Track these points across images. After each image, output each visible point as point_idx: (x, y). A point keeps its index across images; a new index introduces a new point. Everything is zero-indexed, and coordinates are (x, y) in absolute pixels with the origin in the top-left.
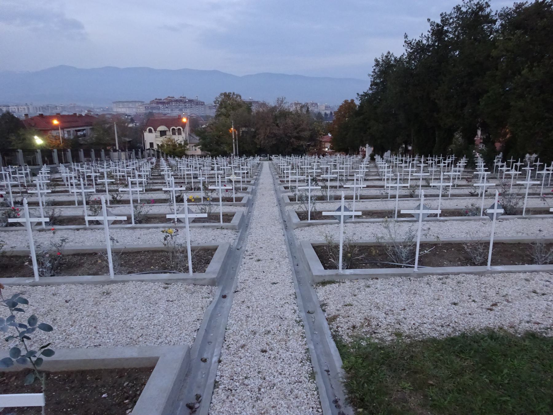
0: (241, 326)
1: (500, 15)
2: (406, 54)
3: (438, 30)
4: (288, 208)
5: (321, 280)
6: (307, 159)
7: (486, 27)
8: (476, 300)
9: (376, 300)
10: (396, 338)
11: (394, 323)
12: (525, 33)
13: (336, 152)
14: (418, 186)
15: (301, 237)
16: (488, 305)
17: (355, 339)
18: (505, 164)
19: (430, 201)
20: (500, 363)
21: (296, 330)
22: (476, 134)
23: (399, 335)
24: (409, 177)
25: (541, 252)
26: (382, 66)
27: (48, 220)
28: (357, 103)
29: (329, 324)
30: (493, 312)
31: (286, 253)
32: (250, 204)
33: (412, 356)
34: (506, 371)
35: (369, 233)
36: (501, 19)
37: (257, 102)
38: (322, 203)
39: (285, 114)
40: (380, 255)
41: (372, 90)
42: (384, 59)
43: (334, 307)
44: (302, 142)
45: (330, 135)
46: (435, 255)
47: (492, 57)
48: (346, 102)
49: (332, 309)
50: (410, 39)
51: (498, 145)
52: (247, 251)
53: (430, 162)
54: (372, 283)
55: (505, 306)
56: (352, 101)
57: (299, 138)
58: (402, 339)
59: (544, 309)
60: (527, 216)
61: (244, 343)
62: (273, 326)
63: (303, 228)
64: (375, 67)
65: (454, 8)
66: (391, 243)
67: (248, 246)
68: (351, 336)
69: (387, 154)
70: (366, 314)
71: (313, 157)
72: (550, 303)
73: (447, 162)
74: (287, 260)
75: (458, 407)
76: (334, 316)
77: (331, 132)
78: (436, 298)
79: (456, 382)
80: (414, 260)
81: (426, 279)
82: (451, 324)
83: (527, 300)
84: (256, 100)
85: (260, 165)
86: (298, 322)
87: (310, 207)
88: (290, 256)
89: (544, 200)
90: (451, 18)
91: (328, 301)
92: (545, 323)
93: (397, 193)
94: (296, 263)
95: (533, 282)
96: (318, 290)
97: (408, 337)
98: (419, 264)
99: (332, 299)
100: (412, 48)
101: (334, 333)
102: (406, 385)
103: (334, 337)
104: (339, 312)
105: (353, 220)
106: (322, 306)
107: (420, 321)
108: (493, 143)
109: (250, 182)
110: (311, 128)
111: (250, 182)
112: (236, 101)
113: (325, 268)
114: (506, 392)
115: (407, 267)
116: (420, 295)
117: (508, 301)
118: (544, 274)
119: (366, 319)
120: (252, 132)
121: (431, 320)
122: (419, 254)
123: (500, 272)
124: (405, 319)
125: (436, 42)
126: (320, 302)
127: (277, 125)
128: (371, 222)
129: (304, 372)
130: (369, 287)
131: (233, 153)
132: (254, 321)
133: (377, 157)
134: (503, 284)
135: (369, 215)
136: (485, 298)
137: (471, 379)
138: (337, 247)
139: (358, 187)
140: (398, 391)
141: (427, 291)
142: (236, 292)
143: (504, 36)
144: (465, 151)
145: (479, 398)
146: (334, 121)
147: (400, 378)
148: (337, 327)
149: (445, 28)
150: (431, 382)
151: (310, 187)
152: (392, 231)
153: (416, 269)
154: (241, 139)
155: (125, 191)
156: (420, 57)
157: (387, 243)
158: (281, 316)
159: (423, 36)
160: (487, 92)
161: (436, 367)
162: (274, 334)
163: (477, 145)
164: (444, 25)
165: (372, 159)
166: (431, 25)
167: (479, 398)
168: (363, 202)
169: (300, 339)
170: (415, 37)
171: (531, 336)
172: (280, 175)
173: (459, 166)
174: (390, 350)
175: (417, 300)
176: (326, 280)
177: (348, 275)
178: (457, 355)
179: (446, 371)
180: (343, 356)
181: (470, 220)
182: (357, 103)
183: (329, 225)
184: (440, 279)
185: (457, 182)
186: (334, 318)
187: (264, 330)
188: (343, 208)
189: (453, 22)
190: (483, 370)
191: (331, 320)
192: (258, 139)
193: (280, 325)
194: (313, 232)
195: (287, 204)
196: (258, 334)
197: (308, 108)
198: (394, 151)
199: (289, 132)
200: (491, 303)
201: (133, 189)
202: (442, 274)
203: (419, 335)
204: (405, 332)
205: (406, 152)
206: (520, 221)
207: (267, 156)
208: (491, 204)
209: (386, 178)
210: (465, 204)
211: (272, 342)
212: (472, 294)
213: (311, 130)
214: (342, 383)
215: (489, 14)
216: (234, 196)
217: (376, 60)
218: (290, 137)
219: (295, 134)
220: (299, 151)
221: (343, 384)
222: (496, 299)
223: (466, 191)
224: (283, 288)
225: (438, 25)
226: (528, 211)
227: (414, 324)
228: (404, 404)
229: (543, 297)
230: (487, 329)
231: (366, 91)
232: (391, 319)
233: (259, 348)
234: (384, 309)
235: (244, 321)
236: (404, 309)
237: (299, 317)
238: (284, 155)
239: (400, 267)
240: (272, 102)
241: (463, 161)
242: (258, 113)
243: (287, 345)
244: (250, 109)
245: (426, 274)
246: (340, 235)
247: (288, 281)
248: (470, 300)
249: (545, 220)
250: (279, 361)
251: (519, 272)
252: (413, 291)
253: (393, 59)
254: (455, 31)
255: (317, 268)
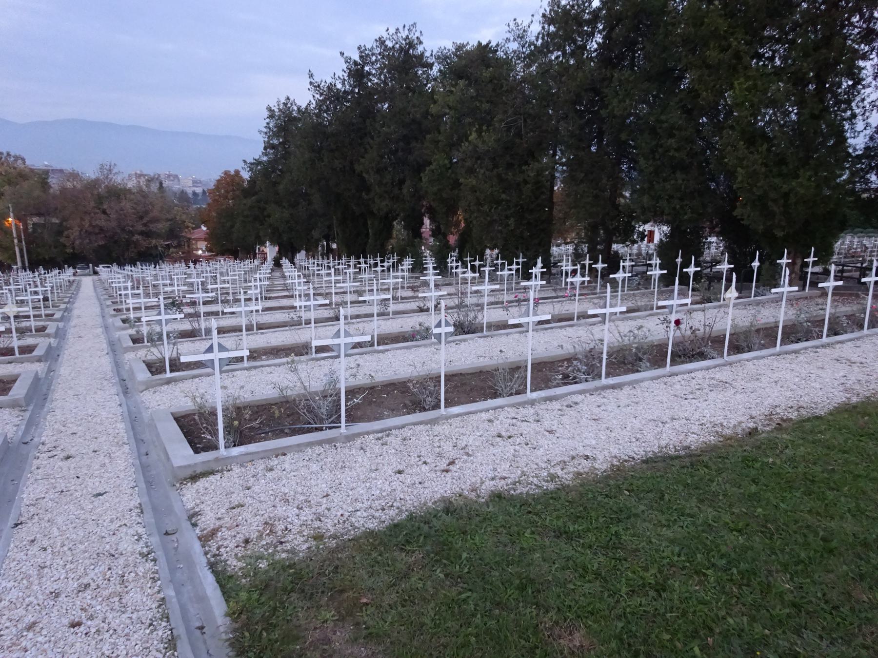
0: (27, 588)
1: (438, 58)
2: (314, 102)
3: (357, 70)
4: (129, 356)
5: (189, 472)
6: (166, 268)
7: (420, 72)
8: (428, 461)
9: (283, 489)
10: (315, 543)
11: (312, 520)
12: (470, 85)
13: (217, 255)
14: (346, 303)
15: (153, 404)
16: (443, 465)
17: (248, 560)
18: (460, 264)
19: (365, 324)
20: (458, 546)
21: (141, 570)
22: (422, 223)
23: (318, 537)
24: (333, 291)
25: (504, 379)
26: (279, 118)
27: (451, 329)
28: (246, 175)
29: (203, 546)
30: (450, 474)
31: (124, 436)
32: (52, 356)
33: (337, 567)
34: (464, 555)
35: (264, 384)
36: (439, 64)
37: (61, 171)
38: (193, 342)
39: (117, 193)
40: (288, 416)
41: (266, 155)
42: (281, 107)
43: (212, 515)
44: (154, 241)
45: (204, 228)
46: (370, 403)
47: (432, 115)
48: (226, 173)
49: (208, 521)
50: (317, 79)
51: (452, 239)
52: (43, 444)
53: (363, 265)
54: (276, 462)
55: (465, 462)
56: (237, 172)
57: (147, 234)
58: (325, 544)
59: (511, 457)
60: (489, 333)
61: (32, 620)
62: (95, 575)
63: (158, 388)
64: (268, 120)
65: (376, 40)
66: (304, 395)
67: (47, 435)
68: (243, 557)
69: (300, 256)
70: (266, 515)
71: (177, 265)
72: (517, 448)
73: (386, 264)
74: (126, 448)
75: (403, 628)
76: (213, 530)
77: (205, 223)
78: (373, 468)
79: (400, 591)
80: (340, 416)
81: (358, 442)
82: (395, 504)
83: (491, 448)
84: (59, 168)
85: (75, 285)
86: (144, 556)
87: (167, 351)
88: (133, 440)
89: (507, 310)
90: (373, 54)
91: (202, 506)
92: (512, 476)
93: (312, 315)
94: (143, 451)
95: (498, 422)
96: (184, 491)
97: (334, 537)
98: (347, 421)
99: (209, 502)
100: (321, 94)
101: (213, 559)
102: (328, 615)
103: (212, 566)
104: (222, 522)
105: (246, 364)
106: (190, 517)
107: (351, 509)
108: (445, 236)
109: (53, 315)
110: (169, 216)
111: (53, 315)
112: (15, 168)
113: (196, 451)
114: (465, 586)
115: (330, 428)
116: (351, 468)
117: (468, 455)
118: (509, 409)
119: (266, 523)
120: (52, 224)
121: (367, 504)
122: (346, 406)
123: (457, 415)
124: (329, 509)
125: (355, 87)
126: (188, 510)
127: (104, 212)
128: (275, 365)
129: (155, 642)
130: (271, 470)
131: (16, 264)
132: (55, 572)
133: (285, 262)
134: (462, 431)
135: (271, 353)
136: (440, 455)
137: (420, 579)
138: (214, 413)
139: (244, 312)
140: (315, 628)
141: (360, 460)
142: (17, 525)
143: (444, 87)
144: (409, 248)
145: (432, 605)
146: (209, 204)
147: (319, 607)
148: (218, 549)
149: (367, 68)
150: (365, 600)
151: (163, 317)
152: (303, 375)
153: (343, 430)
154: (32, 240)
155: (233, 313)
156: (335, 108)
157: (298, 395)
158: (112, 552)
159: (336, 76)
160: (430, 163)
161: (372, 574)
162: (98, 587)
163: (427, 239)
164: (365, 63)
165: (277, 264)
166: (346, 62)
167: (432, 605)
168: (262, 333)
169: (149, 585)
170: (325, 78)
171: (497, 497)
172: (113, 301)
173: (402, 270)
174: (303, 565)
175: (346, 478)
176: (198, 471)
177: (235, 457)
178: (402, 549)
179: (386, 577)
180: (227, 594)
181: (419, 346)
182: (246, 175)
183: (204, 378)
184: (379, 439)
185: (400, 293)
186: (214, 533)
187: (76, 585)
188: (216, 348)
189: (376, 61)
190: (437, 561)
191: (205, 539)
192: (68, 237)
193: (109, 569)
194: (176, 394)
195: (127, 350)
196: (63, 596)
197: (161, 184)
198: (311, 252)
199: (128, 225)
200: (447, 462)
201: (247, 309)
202: (381, 431)
203: (350, 531)
204: (328, 530)
205: (329, 252)
206: (481, 341)
207: (88, 268)
208: (440, 322)
209: (297, 293)
210: (411, 324)
211: (94, 602)
212: (422, 454)
213: (170, 220)
214: (227, 640)
215: (422, 54)
216: (16, 343)
217: (269, 109)
218: (132, 233)
219: (140, 227)
220: (150, 257)
221: (227, 643)
222: (453, 454)
223: (413, 305)
224: (118, 500)
225: (355, 63)
226: (490, 326)
227: (342, 515)
228: (325, 647)
229: (510, 440)
230: (443, 499)
231: (257, 157)
232: (307, 515)
233: (66, 621)
234: (296, 502)
235: (35, 579)
236: (327, 495)
237: (147, 547)
238: (121, 265)
239: (321, 429)
240: (90, 172)
241: (408, 263)
242: (63, 190)
243: (124, 601)
244: (47, 183)
245: (358, 435)
246: (216, 392)
247: (126, 485)
248: (420, 463)
249: (511, 337)
250: (107, 635)
251: (481, 411)
252: (341, 464)
253: (295, 108)
254: (380, 75)
255: (181, 453)
